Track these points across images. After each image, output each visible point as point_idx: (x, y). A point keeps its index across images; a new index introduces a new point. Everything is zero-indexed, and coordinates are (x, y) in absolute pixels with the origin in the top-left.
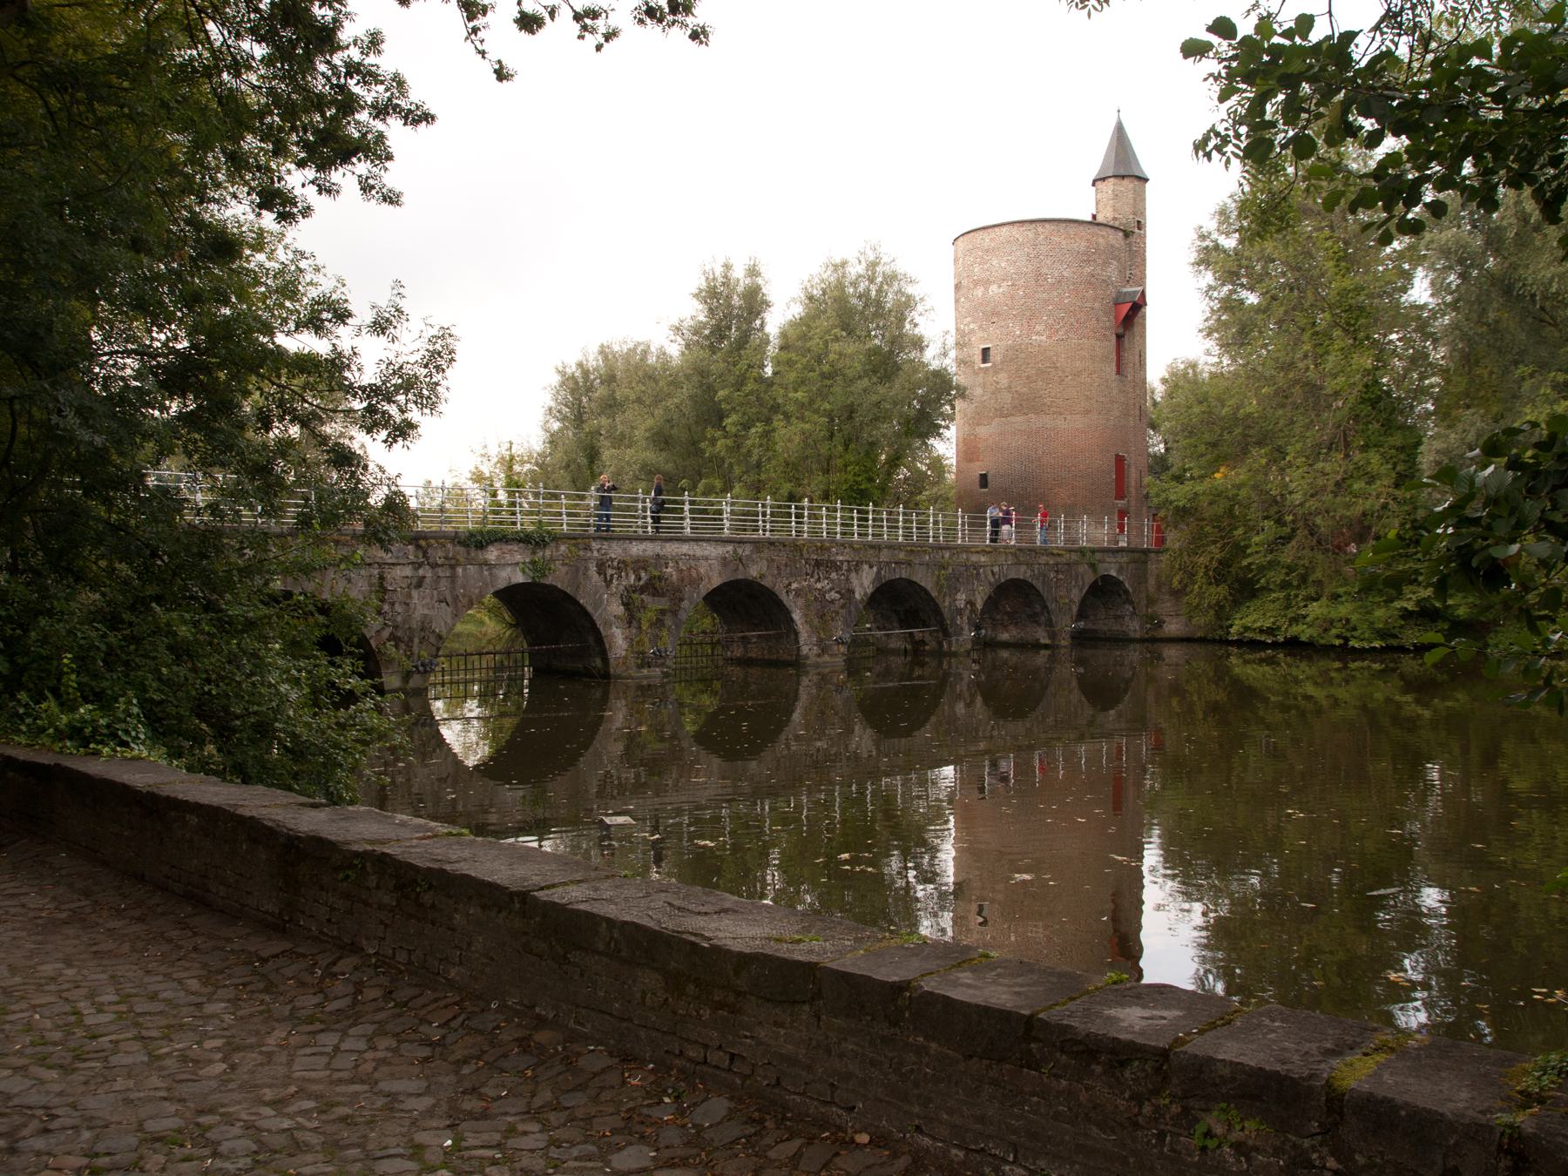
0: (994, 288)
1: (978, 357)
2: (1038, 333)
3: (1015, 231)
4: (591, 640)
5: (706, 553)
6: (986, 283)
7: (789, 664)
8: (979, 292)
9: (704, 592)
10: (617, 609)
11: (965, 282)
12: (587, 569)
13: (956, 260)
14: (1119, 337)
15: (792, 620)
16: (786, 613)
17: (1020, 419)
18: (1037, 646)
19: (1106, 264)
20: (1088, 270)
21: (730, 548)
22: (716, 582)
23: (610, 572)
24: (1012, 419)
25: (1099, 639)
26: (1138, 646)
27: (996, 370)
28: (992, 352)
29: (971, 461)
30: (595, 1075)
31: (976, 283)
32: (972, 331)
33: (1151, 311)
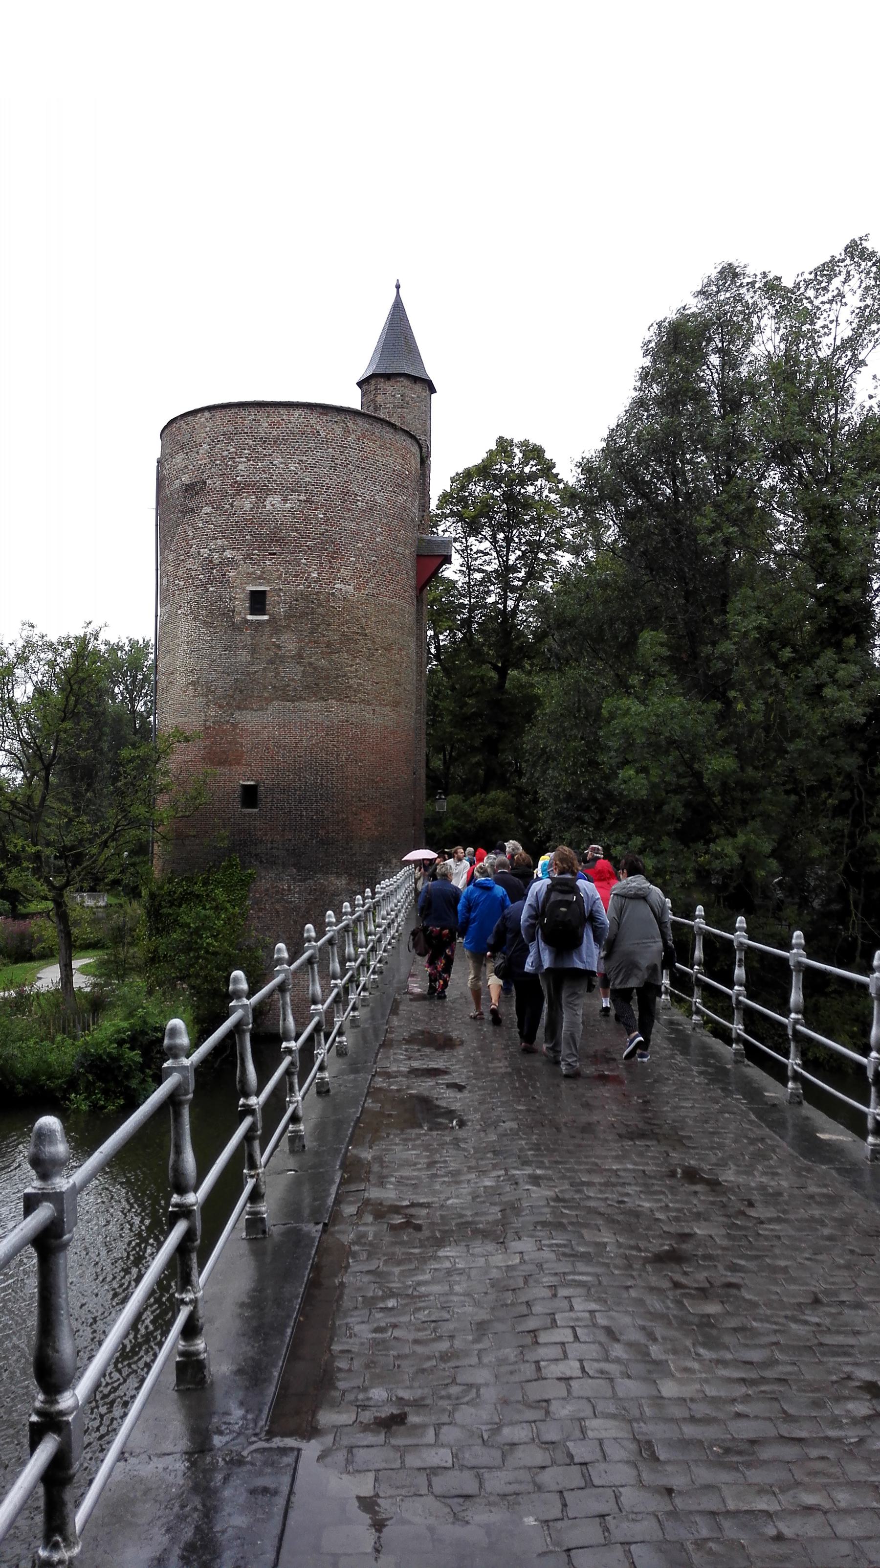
0: (273, 501)
1: (241, 604)
2: (343, 581)
3: (313, 418)
6: (262, 491)
8: (247, 503)
17: (316, 705)
24: (302, 705)
28: (270, 600)
31: (240, 489)
32: (232, 562)
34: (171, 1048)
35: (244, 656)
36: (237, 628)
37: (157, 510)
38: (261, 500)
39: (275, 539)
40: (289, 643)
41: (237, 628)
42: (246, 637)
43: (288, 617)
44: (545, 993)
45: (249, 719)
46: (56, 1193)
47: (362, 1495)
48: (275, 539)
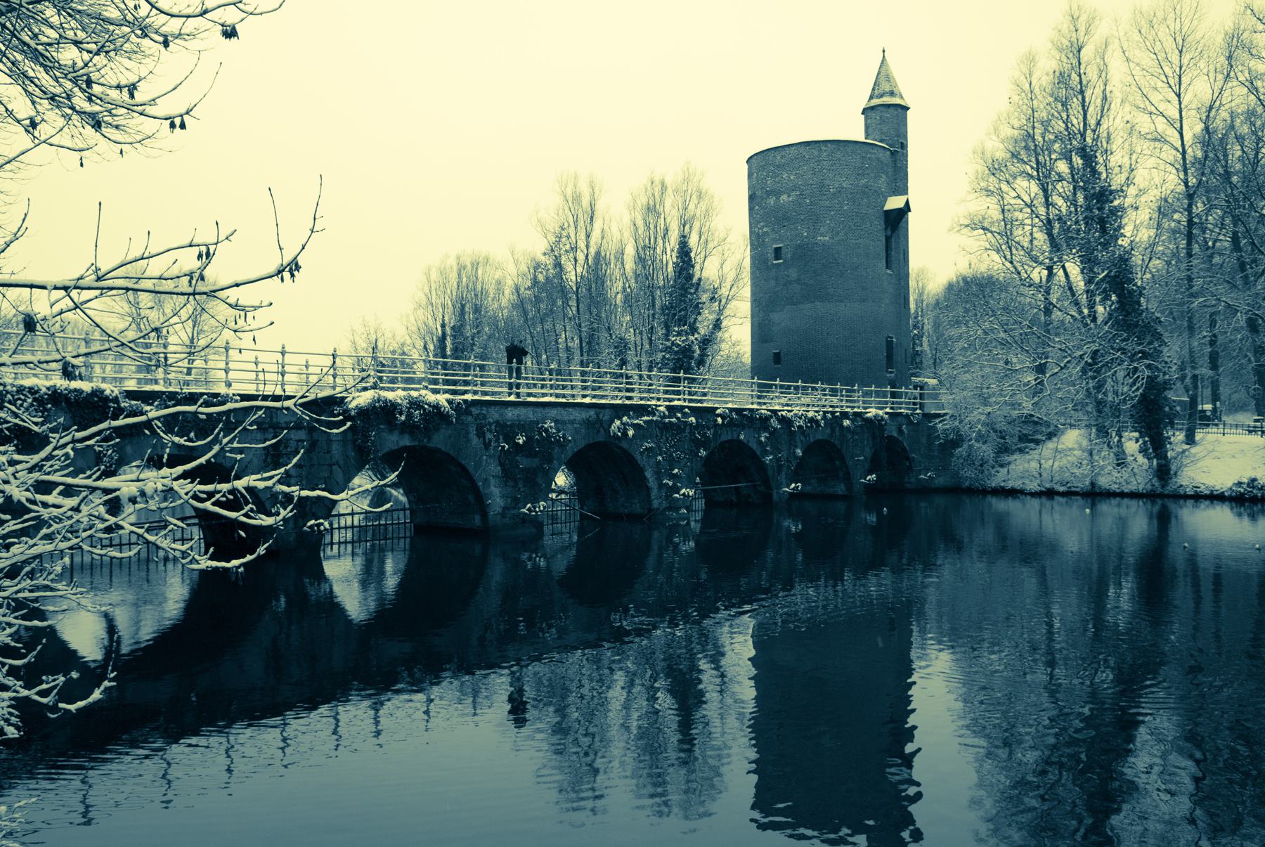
0: (784, 197)
1: (771, 255)
2: (822, 235)
3: (802, 149)
4: (471, 497)
5: (572, 418)
6: (777, 193)
7: (633, 518)
8: (772, 201)
9: (570, 454)
10: (494, 468)
11: (759, 193)
12: (468, 433)
13: (750, 176)
14: (888, 239)
15: (645, 478)
16: (641, 471)
17: (808, 306)
18: (835, 497)
19: (877, 177)
20: (863, 182)
21: (592, 412)
22: (582, 444)
23: (489, 436)
24: (801, 306)
25: (1186, 497)
26: (1061, 499)
27: (786, 265)
28: (783, 251)
29: (766, 341)
30: (73, 108)
31: (768, 194)
32: (765, 234)
33: (914, 221)
34: (1166, 382)
35: (773, 283)
36: (769, 268)
37: (751, 209)
38: (778, 199)
39: (786, 218)
40: (793, 273)
41: (769, 268)
42: (773, 273)
43: (792, 258)
44: (90, 700)
45: (776, 317)
46: (329, 703)
47: (752, 801)
48: (786, 218)
